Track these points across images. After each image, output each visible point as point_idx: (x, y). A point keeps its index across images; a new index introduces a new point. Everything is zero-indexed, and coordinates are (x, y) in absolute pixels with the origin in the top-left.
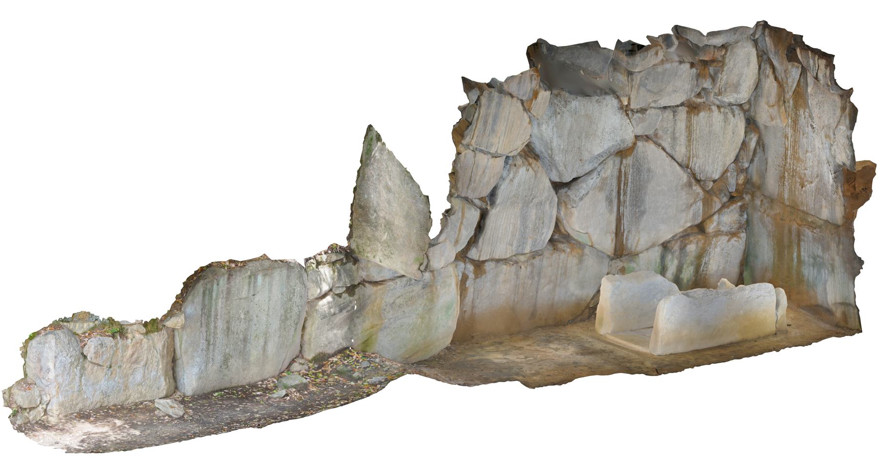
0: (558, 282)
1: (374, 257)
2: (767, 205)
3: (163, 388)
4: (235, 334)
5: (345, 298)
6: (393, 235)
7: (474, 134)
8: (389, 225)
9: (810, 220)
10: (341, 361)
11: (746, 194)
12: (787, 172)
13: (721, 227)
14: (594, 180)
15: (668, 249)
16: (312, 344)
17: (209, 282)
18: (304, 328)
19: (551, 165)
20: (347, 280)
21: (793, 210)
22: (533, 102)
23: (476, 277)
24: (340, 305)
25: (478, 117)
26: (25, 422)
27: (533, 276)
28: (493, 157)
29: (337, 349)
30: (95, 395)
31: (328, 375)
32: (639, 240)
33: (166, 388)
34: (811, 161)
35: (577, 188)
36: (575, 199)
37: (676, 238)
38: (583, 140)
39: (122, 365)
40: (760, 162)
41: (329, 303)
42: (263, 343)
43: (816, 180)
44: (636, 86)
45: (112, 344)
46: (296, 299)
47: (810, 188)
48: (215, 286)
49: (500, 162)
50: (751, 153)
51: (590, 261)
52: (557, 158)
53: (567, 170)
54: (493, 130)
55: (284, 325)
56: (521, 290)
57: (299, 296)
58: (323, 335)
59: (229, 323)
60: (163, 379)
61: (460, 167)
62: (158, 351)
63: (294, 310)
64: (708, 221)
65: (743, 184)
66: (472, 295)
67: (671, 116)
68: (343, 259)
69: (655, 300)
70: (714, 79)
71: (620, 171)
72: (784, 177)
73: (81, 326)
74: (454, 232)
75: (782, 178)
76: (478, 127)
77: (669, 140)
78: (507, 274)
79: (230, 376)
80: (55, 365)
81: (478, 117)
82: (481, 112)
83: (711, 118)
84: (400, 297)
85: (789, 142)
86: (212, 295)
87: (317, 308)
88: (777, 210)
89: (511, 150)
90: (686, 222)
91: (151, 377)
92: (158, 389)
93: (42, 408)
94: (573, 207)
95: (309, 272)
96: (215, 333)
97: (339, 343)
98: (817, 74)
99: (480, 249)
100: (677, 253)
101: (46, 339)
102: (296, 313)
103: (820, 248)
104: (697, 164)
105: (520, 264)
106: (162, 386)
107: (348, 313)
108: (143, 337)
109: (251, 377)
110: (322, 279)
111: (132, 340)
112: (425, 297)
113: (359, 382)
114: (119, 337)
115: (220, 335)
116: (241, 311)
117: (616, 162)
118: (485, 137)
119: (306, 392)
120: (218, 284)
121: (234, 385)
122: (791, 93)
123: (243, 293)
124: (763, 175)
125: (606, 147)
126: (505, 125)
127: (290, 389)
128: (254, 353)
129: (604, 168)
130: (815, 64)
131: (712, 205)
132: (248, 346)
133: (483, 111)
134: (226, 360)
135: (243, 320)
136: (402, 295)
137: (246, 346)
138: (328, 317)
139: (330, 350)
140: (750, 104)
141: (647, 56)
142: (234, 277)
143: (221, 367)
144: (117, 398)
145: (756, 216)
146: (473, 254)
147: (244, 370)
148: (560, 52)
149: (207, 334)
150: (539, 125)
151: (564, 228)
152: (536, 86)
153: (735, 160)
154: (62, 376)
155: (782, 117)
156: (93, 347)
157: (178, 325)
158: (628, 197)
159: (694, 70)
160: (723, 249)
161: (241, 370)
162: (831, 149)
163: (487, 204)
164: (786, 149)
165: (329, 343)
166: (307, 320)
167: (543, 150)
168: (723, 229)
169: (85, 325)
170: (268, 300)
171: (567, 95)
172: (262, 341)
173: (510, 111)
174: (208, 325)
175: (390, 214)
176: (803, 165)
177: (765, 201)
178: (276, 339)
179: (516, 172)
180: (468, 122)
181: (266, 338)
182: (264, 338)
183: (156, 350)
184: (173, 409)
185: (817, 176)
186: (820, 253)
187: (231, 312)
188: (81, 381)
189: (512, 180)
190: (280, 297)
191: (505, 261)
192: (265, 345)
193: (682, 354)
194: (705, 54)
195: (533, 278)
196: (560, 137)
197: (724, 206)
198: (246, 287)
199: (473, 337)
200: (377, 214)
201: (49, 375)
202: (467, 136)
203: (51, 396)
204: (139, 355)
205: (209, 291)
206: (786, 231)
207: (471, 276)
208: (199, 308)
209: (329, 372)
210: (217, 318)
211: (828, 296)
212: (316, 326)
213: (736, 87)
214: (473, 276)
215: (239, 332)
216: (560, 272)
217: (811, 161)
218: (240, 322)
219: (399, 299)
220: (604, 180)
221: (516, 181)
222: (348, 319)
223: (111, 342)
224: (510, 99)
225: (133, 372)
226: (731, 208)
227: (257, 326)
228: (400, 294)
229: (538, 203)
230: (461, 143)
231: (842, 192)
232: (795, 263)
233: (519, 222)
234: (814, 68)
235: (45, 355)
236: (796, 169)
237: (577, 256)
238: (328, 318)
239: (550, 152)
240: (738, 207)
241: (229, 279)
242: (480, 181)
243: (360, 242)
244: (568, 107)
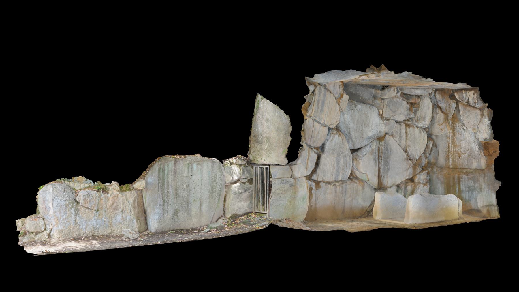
0: (354, 197)
1: (261, 159)
2: (440, 170)
3: (135, 227)
4: (181, 197)
5: (247, 185)
6: (270, 144)
7: (313, 110)
8: (268, 139)
9: (464, 171)
10: (246, 218)
11: (429, 167)
12: (450, 153)
13: (420, 180)
14: (369, 148)
15: (400, 187)
16: (229, 209)
17: (162, 164)
18: (225, 200)
19: (349, 138)
20: (248, 175)
21: (454, 170)
22: (341, 99)
23: (316, 189)
24: (245, 188)
25: (315, 100)
26: (31, 241)
27: (343, 192)
28: (322, 126)
29: (244, 213)
30: (88, 228)
31: (238, 224)
32: (388, 181)
33: (138, 226)
34: (464, 144)
35: (361, 151)
36: (361, 155)
37: (402, 183)
38: (364, 127)
39: (106, 210)
40: (434, 153)
41: (238, 186)
42: (199, 205)
43: (468, 152)
44: (386, 106)
45: (96, 196)
46: (218, 181)
47: (464, 156)
48: (166, 167)
49: (326, 129)
50: (430, 150)
51: (367, 189)
52: (352, 134)
53: (357, 141)
54: (322, 110)
55: (212, 196)
56: (337, 199)
57: (219, 180)
58: (235, 204)
59: (177, 191)
60: (135, 221)
61: (307, 127)
62: (130, 203)
63: (217, 188)
64: (415, 177)
65: (427, 164)
66: (315, 198)
67: (399, 126)
68: (245, 163)
69: (399, 205)
70: (415, 113)
71: (379, 148)
72: (448, 156)
73: (78, 185)
74: (305, 163)
75: (447, 156)
76: (315, 106)
77: (398, 137)
78: (331, 190)
79: (179, 223)
80: (53, 205)
81: (315, 100)
82: (316, 98)
83: (414, 131)
84: (278, 189)
85: (450, 140)
86: (164, 172)
87: (231, 188)
88: (445, 171)
89: (331, 124)
90: (406, 176)
91: (127, 219)
92: (133, 227)
93: (46, 233)
94: (360, 160)
95: (226, 168)
96: (168, 196)
97: (245, 209)
98: (468, 100)
99: (318, 174)
100: (403, 190)
101: (47, 188)
102: (219, 190)
103: (472, 182)
104: (410, 150)
105: (337, 186)
106: (135, 226)
107: (249, 193)
108: (119, 193)
109: (193, 224)
110: (234, 173)
111: (111, 194)
112: (291, 191)
113: (254, 226)
114: (102, 192)
115: (171, 197)
116: (184, 184)
117: (377, 143)
118: (318, 113)
119: (222, 231)
120: (168, 166)
121: (182, 228)
122: (451, 116)
123: (185, 173)
124: (436, 158)
125: (373, 133)
126: (328, 108)
127: (213, 229)
128: (194, 210)
129: (372, 144)
130: (467, 95)
131: (416, 170)
132: (190, 206)
133: (317, 96)
134: (176, 212)
135: (185, 190)
136: (279, 189)
137: (189, 206)
138: (238, 194)
139: (240, 213)
140: (429, 129)
141: (390, 90)
142: (178, 163)
143: (173, 216)
144: (104, 231)
145: (434, 176)
146: (315, 177)
147: (188, 220)
148: (350, 87)
149: (162, 196)
150: (343, 114)
151: (355, 174)
152: (342, 91)
153: (424, 152)
154: (60, 213)
155: (448, 127)
156: (82, 196)
157: (142, 187)
158: (383, 160)
159: (408, 105)
160: (421, 190)
161: (186, 219)
162: (475, 136)
163: (320, 152)
164: (449, 143)
165: (239, 209)
166: (226, 196)
167: (345, 130)
168: (421, 181)
169: (82, 185)
170: (200, 179)
171: (356, 102)
172: (198, 203)
173: (330, 100)
174: (163, 190)
175: (269, 133)
176: (459, 147)
177: (438, 169)
178: (207, 203)
179: (334, 137)
180: (310, 103)
181: (201, 202)
182: (200, 202)
183: (128, 202)
184: (131, 234)
185: (468, 150)
186: (472, 184)
187: (178, 184)
188: (76, 218)
189: (332, 141)
190: (208, 179)
191: (329, 183)
192: (200, 206)
193: (421, 224)
194: (412, 99)
195: (343, 193)
196: (353, 123)
197: (420, 172)
198: (186, 170)
199: (316, 219)
200: (262, 136)
201: (50, 212)
202: (309, 110)
203: (53, 225)
204: (117, 205)
205: (162, 169)
206: (452, 179)
207: (314, 188)
208: (156, 179)
209: (238, 223)
210: (169, 187)
211: (478, 204)
212: (231, 198)
213: (424, 118)
214: (315, 188)
215: (183, 196)
216: (354, 192)
217: (464, 144)
218: (184, 191)
219: (278, 190)
220: (372, 150)
221: (334, 141)
222: (250, 197)
223: (96, 194)
224: (330, 93)
225: (115, 215)
226: (423, 172)
227: (195, 194)
228: (278, 188)
229: (344, 156)
230: (306, 115)
231: (484, 153)
232: (457, 192)
233: (335, 164)
234: (466, 98)
235: (47, 198)
236: (455, 150)
237: (362, 186)
238: (238, 195)
239: (349, 130)
240: (426, 173)
241: (175, 164)
242: (317, 138)
243: (254, 154)
244: (357, 108)
